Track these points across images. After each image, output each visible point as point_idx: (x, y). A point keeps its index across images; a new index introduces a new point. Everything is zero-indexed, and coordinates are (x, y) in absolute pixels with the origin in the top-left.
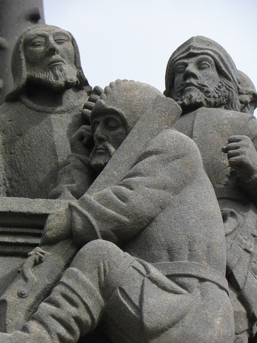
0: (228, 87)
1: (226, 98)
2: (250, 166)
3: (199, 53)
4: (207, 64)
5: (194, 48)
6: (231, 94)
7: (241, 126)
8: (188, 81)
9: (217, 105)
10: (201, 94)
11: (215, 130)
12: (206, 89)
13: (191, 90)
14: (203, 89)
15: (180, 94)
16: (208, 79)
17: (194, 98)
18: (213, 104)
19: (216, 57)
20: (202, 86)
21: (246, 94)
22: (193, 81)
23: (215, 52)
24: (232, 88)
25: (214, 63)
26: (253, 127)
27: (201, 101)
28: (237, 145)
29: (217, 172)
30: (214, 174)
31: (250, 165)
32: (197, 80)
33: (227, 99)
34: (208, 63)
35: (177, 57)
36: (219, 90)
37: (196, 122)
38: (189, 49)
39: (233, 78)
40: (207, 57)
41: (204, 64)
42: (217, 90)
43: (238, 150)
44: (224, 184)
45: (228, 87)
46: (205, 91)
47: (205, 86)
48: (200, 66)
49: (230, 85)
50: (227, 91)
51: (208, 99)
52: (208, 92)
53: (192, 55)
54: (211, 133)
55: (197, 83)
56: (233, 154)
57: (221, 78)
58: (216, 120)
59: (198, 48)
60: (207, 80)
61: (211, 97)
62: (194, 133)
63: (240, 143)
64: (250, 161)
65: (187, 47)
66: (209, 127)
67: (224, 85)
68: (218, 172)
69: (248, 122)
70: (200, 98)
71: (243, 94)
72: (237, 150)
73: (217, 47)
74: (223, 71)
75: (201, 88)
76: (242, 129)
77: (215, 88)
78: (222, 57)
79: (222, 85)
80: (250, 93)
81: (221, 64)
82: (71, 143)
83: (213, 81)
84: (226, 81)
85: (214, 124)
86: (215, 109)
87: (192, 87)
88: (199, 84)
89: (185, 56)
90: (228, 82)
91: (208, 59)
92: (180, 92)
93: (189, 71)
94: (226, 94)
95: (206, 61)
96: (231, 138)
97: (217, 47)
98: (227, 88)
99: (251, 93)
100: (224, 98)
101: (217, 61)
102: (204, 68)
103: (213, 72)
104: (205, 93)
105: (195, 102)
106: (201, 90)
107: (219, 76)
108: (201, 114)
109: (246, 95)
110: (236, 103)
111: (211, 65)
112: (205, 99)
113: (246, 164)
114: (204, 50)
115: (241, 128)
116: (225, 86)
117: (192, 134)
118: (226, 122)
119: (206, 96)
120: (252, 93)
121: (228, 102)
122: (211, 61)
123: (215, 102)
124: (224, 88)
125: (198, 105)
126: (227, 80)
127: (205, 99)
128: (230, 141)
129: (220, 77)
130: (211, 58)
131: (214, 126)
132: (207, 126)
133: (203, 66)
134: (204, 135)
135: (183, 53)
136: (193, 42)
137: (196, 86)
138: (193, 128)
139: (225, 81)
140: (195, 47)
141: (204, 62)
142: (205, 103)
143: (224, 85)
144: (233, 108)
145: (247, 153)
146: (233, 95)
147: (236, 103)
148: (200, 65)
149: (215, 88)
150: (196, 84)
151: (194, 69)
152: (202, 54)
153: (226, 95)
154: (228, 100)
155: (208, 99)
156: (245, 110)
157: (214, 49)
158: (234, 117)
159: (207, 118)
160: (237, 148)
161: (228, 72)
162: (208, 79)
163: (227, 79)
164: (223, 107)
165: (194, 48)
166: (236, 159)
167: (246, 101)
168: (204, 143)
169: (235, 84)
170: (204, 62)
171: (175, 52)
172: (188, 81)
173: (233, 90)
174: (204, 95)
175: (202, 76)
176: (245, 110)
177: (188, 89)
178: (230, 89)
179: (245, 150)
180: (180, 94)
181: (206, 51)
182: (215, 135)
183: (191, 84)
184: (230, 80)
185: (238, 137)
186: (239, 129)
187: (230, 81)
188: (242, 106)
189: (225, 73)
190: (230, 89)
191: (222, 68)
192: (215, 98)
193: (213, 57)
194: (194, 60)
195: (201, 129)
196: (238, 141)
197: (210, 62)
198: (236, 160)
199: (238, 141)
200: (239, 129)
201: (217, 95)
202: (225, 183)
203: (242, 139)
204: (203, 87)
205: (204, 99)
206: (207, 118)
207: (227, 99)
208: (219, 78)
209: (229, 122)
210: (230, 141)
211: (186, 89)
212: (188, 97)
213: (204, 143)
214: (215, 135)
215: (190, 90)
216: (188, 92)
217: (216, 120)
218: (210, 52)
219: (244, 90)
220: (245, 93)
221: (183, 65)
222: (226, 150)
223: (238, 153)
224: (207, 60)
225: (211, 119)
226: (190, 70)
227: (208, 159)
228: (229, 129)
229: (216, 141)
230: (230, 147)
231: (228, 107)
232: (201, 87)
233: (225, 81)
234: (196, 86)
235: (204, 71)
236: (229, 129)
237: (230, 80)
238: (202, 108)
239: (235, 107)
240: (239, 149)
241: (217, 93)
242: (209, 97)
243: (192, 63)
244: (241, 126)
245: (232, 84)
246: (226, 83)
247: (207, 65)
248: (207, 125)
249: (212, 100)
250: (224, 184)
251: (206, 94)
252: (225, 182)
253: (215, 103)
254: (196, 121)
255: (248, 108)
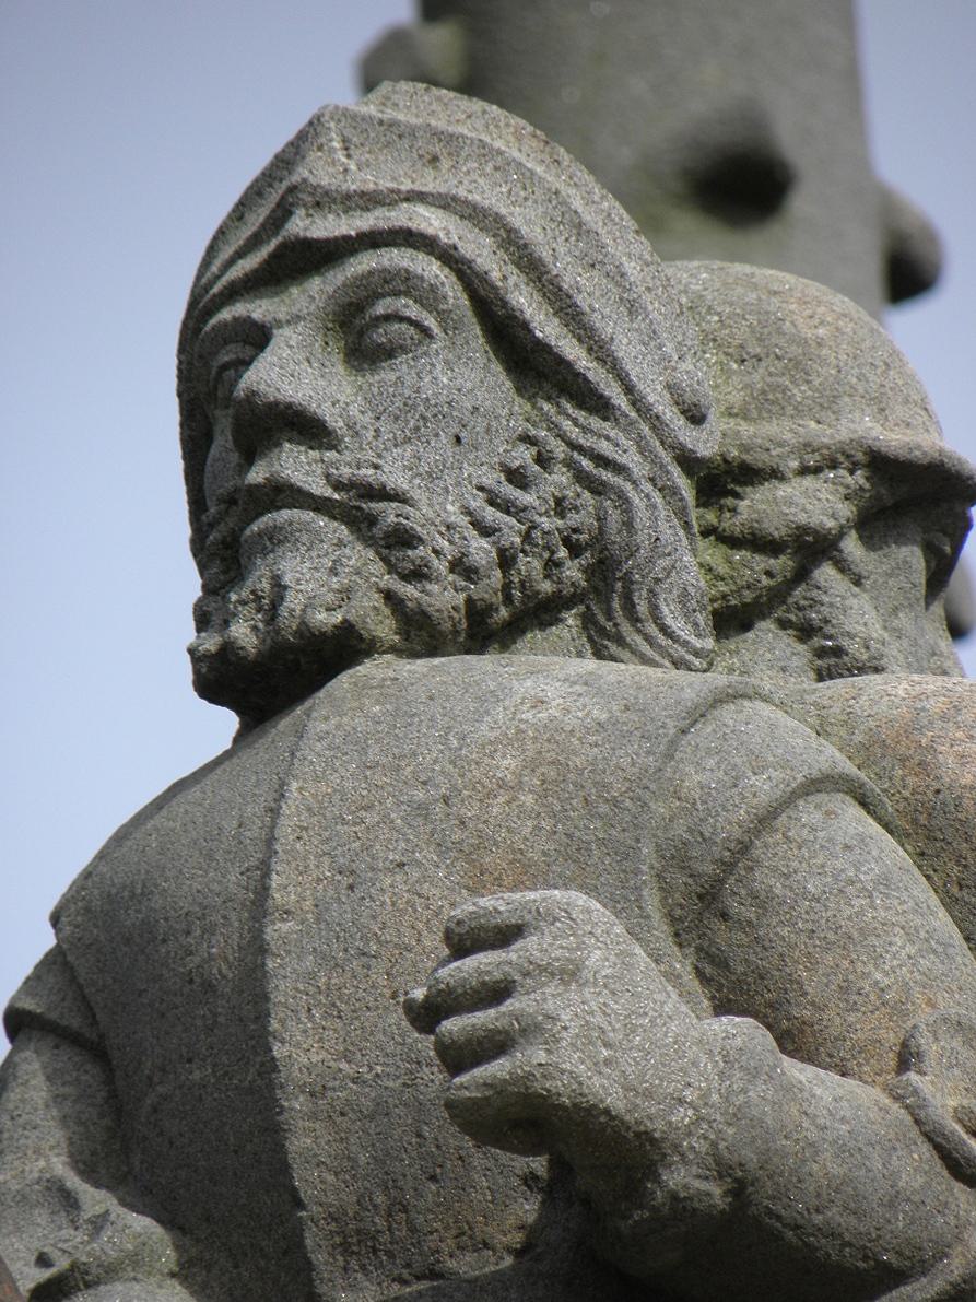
0: (586, 464)
1: (575, 550)
2: (603, 1119)
3: (346, 238)
4: (407, 313)
5: (318, 204)
6: (614, 518)
7: (618, 788)
8: (257, 475)
9: (483, 631)
10: (359, 556)
11: (428, 843)
12: (389, 513)
13: (280, 541)
14: (372, 520)
15: (225, 572)
16: (417, 429)
17: (293, 602)
18: (447, 626)
19: (481, 251)
20: (361, 497)
21: (804, 471)
22: (296, 464)
23: (475, 215)
24: (619, 469)
25: (465, 301)
26: (720, 774)
27: (345, 621)
28: (498, 975)
29: (449, 1165)
30: (433, 1178)
31: (607, 1112)
32: (330, 455)
33: (588, 558)
34: (413, 310)
35: (218, 277)
36: (507, 507)
37: (301, 789)
38: (283, 213)
39: (629, 389)
40: (405, 263)
41: (388, 318)
42: (492, 503)
43: (502, 1008)
44: (509, 1250)
45: (586, 464)
46: (387, 535)
47: (383, 494)
48: (360, 336)
49: (604, 448)
50: (587, 494)
51: (409, 591)
52: (403, 538)
53: (300, 261)
54: (401, 865)
55: (327, 476)
56: (469, 1041)
57: (534, 406)
58: (435, 761)
59: (348, 197)
60: (408, 440)
61: (426, 577)
62: (275, 880)
63: (512, 954)
64: (597, 1082)
65: (273, 197)
66: (386, 819)
67: (559, 450)
68: (461, 1158)
69: (673, 743)
70: (346, 594)
71: (776, 474)
72: (492, 1012)
73: (496, 169)
74: (543, 347)
75: (360, 507)
76: (628, 803)
77: (481, 488)
78: (525, 246)
79: (543, 460)
80: (841, 459)
81: (524, 300)
82: (256, 727)
83: (458, 440)
84: (572, 421)
85: (420, 795)
86: (485, 665)
87: (285, 514)
88: (338, 486)
89: (255, 271)
90: (585, 430)
91: (408, 276)
92: (223, 559)
93: (254, 393)
94: (574, 519)
95: (397, 294)
96: (459, 923)
97: (496, 169)
98: (581, 477)
99: (848, 456)
100: (563, 553)
101: (484, 278)
102: (388, 352)
103: (462, 374)
104: (388, 547)
105: (299, 633)
106: (359, 530)
107: (520, 391)
108: (338, 727)
109: (808, 482)
110: (657, 581)
111: (443, 317)
112: (389, 596)
113: (562, 1107)
114: (392, 204)
115: (615, 803)
116: (569, 464)
117: (266, 888)
118: (507, 764)
119: (391, 568)
120: (860, 456)
121: (605, 579)
122: (433, 288)
123: (469, 601)
124: (560, 478)
125: (340, 650)
126: (581, 415)
127: (389, 596)
128: (462, 943)
129: (531, 399)
130: (430, 269)
131: (422, 810)
132: (371, 818)
133: (379, 336)
134: (351, 887)
135: (240, 254)
136: (320, 148)
137: (320, 505)
138: (270, 840)
139: (567, 425)
140: (326, 193)
141: (380, 308)
142: (384, 627)
143: (559, 450)
144: (638, 620)
145: (565, 1028)
146: (629, 525)
147: (657, 581)
148: (361, 334)
149: (481, 488)
150: (320, 488)
151: (308, 372)
152: (373, 240)
153: (575, 531)
154: (601, 562)
155: (409, 591)
156: (815, 593)
157: (462, 193)
158: (570, 722)
159: (373, 753)
160: (497, 992)
161: (590, 350)
162: (417, 429)
163: (581, 405)
164: (570, 622)
165: (324, 201)
166: (485, 1084)
167: (798, 528)
168: (346, 950)
169: (653, 428)
170: (380, 308)
171: (222, 234)
172: (257, 475)
173: (628, 486)
174: (377, 567)
175: (368, 418)
176: (815, 593)
177: (259, 535)
178: (606, 475)
179: (550, 1005)
180: (225, 572)
181: (399, 217)
182: (424, 878)
183: (282, 494)
184: (599, 405)
185: (498, 904)
186: (604, 808)
187: (605, 419)
188: (769, 574)
189: (562, 362)
190: (606, 475)
191: (530, 332)
192: (463, 568)
193: (448, 257)
194: (317, 291)
195: (326, 848)
196: (506, 935)
197: (429, 297)
198: (489, 1093)
199: (506, 935)
200: (604, 808)
201: (481, 550)
202: (517, 1239)
203: (528, 917)
204: (372, 505)
205: (377, 600)
206: (373, 753)
207: (588, 558)
208: (521, 405)
209: (532, 765)
210: (462, 943)
211: (248, 532)
212: (258, 598)
213: (346, 950)
214: (424, 878)
215: (274, 539)
216: (265, 552)
217: (435, 761)
218: (430, 221)
219: (781, 444)
220: (795, 464)
221: (245, 342)
222: (427, 1015)
223: (500, 1032)
224: (405, 283)
225: (403, 757)
226: (262, 387)
227: (379, 1069)
228: (529, 824)
229: (429, 929)
230: (450, 991)
231: (601, 619)
232: (359, 508)
233: (567, 425)
234: (320, 505)
235: (386, 375)
236: (529, 824)
237: (599, 405)
238: (366, 668)
239: (654, 609)
240: (509, 1005)
241: (485, 531)
242: (418, 575)
243: (295, 319)
244: (618, 788)
245: (623, 441)
246: (574, 433)
247: (404, 326)
248: (367, 808)
249: (443, 598)
250: (509, 1250)
251: (396, 554)
252: (522, 1227)
253: (477, 613)
254: (295, 785)
255: (842, 570)
